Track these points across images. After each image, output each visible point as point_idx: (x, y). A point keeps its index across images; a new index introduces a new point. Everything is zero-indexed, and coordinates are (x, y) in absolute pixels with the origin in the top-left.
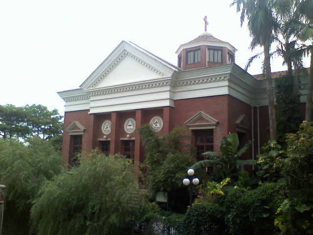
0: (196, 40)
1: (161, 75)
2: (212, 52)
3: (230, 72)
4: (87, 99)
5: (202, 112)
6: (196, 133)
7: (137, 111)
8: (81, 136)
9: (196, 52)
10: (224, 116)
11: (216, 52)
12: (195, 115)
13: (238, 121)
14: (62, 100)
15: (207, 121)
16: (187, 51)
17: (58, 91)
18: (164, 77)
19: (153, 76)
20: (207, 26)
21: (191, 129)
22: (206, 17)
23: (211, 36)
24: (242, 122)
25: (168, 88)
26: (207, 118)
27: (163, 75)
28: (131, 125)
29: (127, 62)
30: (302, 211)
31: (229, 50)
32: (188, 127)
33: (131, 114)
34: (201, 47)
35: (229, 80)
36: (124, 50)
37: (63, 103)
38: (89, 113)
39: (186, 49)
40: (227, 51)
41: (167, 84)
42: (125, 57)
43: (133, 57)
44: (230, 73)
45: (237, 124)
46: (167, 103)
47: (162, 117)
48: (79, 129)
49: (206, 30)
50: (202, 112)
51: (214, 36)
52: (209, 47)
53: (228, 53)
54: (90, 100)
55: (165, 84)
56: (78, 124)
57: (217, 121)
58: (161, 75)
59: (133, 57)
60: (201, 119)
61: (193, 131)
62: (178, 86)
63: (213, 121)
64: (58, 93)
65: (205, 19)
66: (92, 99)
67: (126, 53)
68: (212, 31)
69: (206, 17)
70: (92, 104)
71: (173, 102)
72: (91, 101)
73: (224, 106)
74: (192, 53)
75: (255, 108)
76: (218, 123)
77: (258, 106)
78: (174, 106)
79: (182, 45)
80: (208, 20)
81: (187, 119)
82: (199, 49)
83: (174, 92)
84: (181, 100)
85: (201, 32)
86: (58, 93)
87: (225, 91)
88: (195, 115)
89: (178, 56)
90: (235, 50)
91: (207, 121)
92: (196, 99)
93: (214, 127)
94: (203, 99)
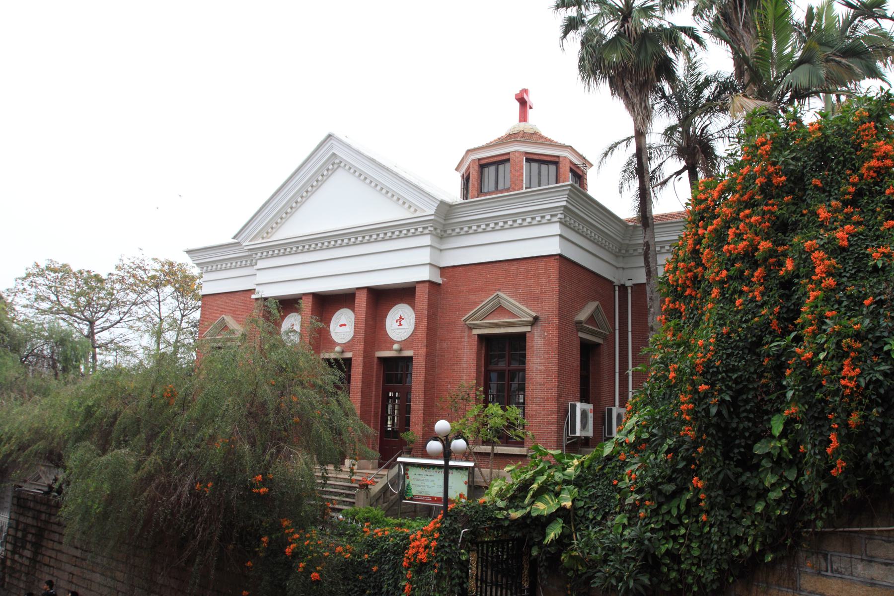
0: (501, 142)
1: (412, 209)
2: (535, 166)
3: (564, 203)
4: (251, 265)
5: (501, 294)
6: (486, 341)
7: (417, 286)
9: (501, 167)
10: (550, 305)
11: (544, 167)
12: (486, 301)
13: (583, 316)
15: (514, 316)
16: (483, 165)
18: (418, 214)
19: (390, 213)
20: (530, 112)
21: (476, 332)
23: (536, 133)
24: (591, 319)
25: (427, 240)
27: (416, 211)
28: (345, 325)
29: (340, 181)
31: (571, 162)
32: (470, 328)
33: (344, 299)
34: (511, 157)
35: (562, 223)
36: (334, 154)
38: (253, 296)
39: (479, 160)
40: (568, 166)
41: (426, 231)
42: (334, 171)
43: (350, 168)
44: (565, 207)
45: (580, 322)
46: (424, 274)
47: (412, 305)
49: (523, 117)
50: (501, 294)
51: (545, 133)
52: (573, 167)
53: (571, 170)
54: (256, 267)
55: (420, 230)
57: (534, 314)
58: (412, 209)
59: (350, 168)
60: (500, 309)
61: (480, 336)
62: (450, 236)
63: (526, 312)
66: (261, 264)
67: (337, 161)
68: (537, 121)
70: (262, 277)
71: (438, 272)
72: (258, 270)
73: (550, 279)
74: (492, 169)
75: (623, 288)
76: (536, 319)
77: (629, 284)
79: (468, 151)
80: (531, 99)
81: (467, 311)
82: (508, 160)
83: (441, 250)
84: (448, 267)
85: (509, 121)
86: (189, 252)
87: (553, 247)
88: (486, 301)
90: (587, 163)
91: (514, 316)
92: (514, 267)
93: (528, 329)
94: (474, 267)
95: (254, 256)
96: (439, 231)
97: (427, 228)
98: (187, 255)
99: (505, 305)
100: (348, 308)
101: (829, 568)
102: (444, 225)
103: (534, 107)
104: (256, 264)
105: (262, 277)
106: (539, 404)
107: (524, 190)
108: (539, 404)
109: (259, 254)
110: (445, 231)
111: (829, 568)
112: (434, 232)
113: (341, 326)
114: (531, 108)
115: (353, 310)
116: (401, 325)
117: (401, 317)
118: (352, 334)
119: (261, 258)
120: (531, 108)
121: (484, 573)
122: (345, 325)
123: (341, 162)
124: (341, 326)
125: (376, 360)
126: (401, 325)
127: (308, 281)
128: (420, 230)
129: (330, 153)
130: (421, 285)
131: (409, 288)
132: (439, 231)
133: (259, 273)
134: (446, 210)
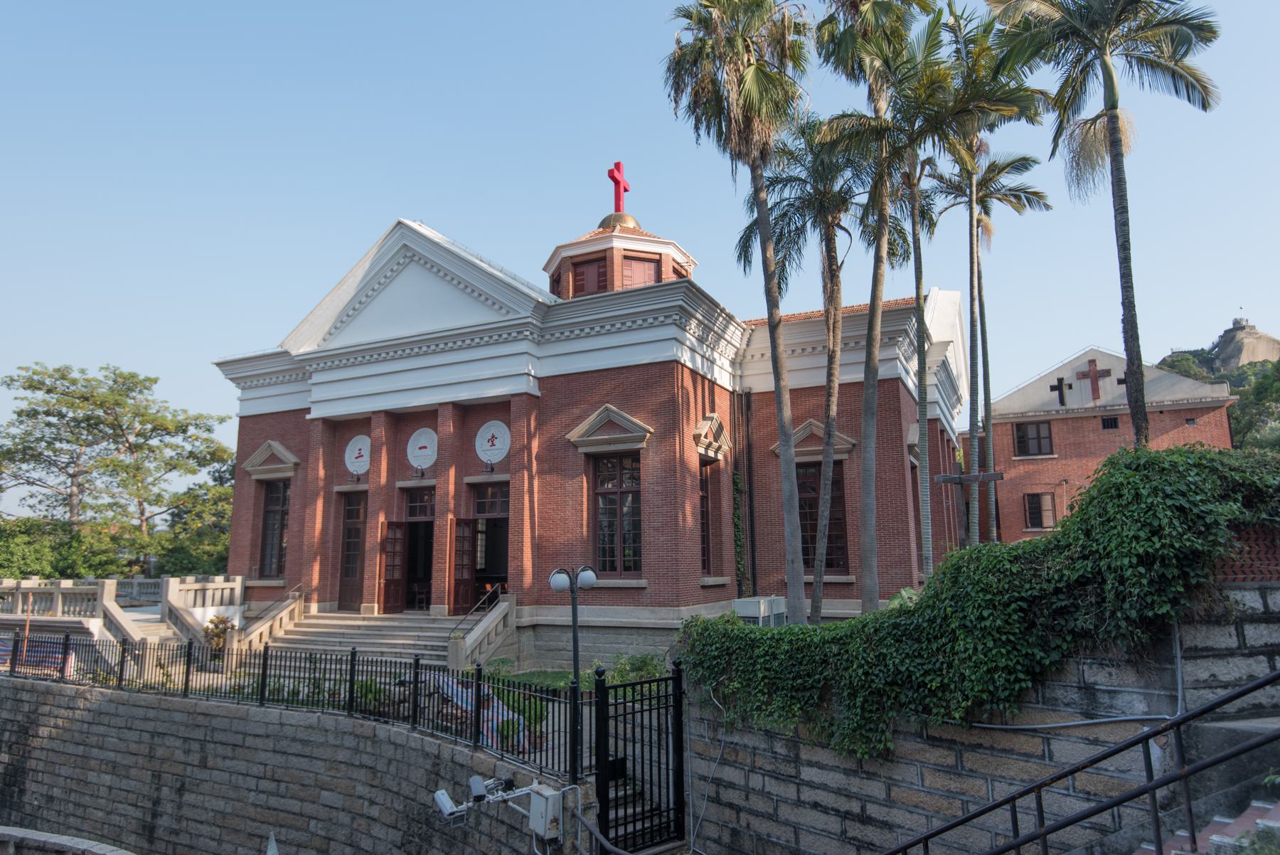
1: (504, 311)
8: (286, 483)
14: (232, 385)
15: (625, 430)
17: (221, 360)
18: (510, 316)
20: (625, 196)
22: (618, 166)
26: (284, 459)
27: (508, 312)
28: (425, 447)
30: (809, 601)
33: (426, 416)
37: (233, 391)
38: (308, 417)
48: (282, 462)
52: (676, 266)
54: (310, 382)
56: (278, 447)
60: (273, 458)
61: (587, 455)
64: (218, 365)
65: (614, 175)
66: (317, 378)
69: (618, 166)
70: (317, 394)
78: (538, 394)
80: (626, 176)
86: (218, 365)
89: (552, 276)
91: (625, 430)
95: (308, 368)
96: (535, 336)
97: (522, 332)
98: (217, 368)
99: (616, 419)
100: (429, 427)
101: (1040, 699)
102: (541, 329)
103: (631, 188)
104: (310, 377)
105: (317, 394)
106: (656, 529)
107: (571, 300)
108: (656, 529)
109: (315, 366)
110: (543, 336)
111: (1040, 699)
112: (530, 337)
113: (420, 448)
114: (626, 190)
115: (436, 430)
116: (493, 445)
117: (493, 436)
118: (435, 457)
119: (316, 371)
120: (626, 190)
121: (527, 702)
122: (425, 447)
123: (414, 255)
124: (420, 448)
125: (397, 490)
126: (493, 445)
127: (329, 403)
128: (514, 334)
129: (401, 245)
130: (517, 398)
131: (423, 412)
132: (535, 336)
133: (314, 389)
134: (543, 310)
